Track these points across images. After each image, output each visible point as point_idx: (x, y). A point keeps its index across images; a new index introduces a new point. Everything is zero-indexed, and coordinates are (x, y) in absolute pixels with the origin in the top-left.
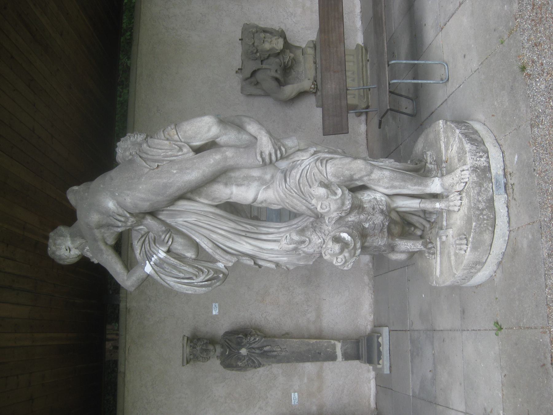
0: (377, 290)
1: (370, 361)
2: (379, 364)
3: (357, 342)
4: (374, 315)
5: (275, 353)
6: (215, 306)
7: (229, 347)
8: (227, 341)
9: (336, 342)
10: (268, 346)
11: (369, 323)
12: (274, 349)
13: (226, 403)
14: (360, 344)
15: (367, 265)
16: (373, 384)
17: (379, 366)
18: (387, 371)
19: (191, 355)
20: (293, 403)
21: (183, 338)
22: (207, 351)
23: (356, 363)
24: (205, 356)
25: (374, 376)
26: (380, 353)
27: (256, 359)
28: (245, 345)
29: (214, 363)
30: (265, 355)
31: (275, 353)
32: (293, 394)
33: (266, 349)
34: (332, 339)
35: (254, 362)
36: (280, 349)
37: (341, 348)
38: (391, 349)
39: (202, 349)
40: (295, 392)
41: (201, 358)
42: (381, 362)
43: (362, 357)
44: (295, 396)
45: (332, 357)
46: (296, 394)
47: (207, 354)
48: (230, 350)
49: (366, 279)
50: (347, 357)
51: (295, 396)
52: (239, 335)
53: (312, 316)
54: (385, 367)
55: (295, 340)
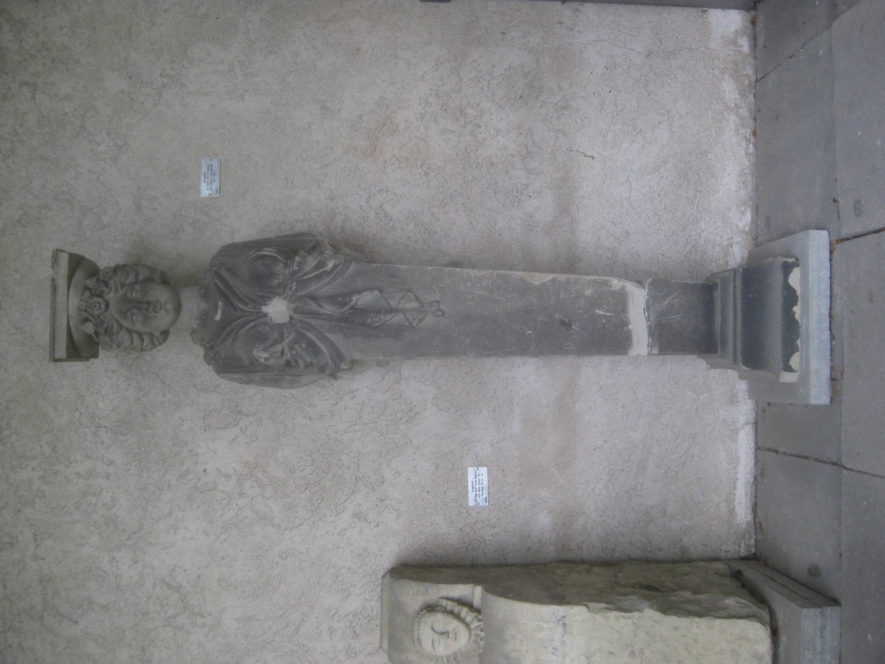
0: (765, 122)
1: (752, 357)
2: (789, 369)
3: (707, 291)
4: (756, 211)
5: (398, 319)
6: (210, 167)
7: (227, 294)
8: (224, 273)
9: (630, 287)
10: (371, 289)
11: (737, 239)
12: (393, 303)
13: (241, 495)
14: (717, 294)
15: (734, 42)
16: (744, 445)
17: (788, 378)
18: (818, 394)
19: (86, 320)
20: (471, 503)
21: (55, 260)
22: (146, 307)
23: (692, 367)
24: (139, 327)
25: (751, 417)
26: (791, 328)
27: (326, 340)
28: (283, 286)
29: (183, 358)
30: (355, 321)
31: (398, 319)
32: (471, 471)
33: (364, 299)
34: (612, 273)
35: (314, 350)
36: (414, 304)
37: (648, 308)
38: (837, 309)
39: (125, 299)
40: (478, 465)
41: (123, 336)
42: (795, 361)
43: (724, 343)
44: (478, 481)
45: (611, 340)
46: (484, 470)
47: (146, 320)
48: (229, 303)
49: (729, 89)
50: (668, 340)
51: (478, 481)
52: (260, 249)
53: (542, 206)
54: (813, 380)
55: (473, 273)
